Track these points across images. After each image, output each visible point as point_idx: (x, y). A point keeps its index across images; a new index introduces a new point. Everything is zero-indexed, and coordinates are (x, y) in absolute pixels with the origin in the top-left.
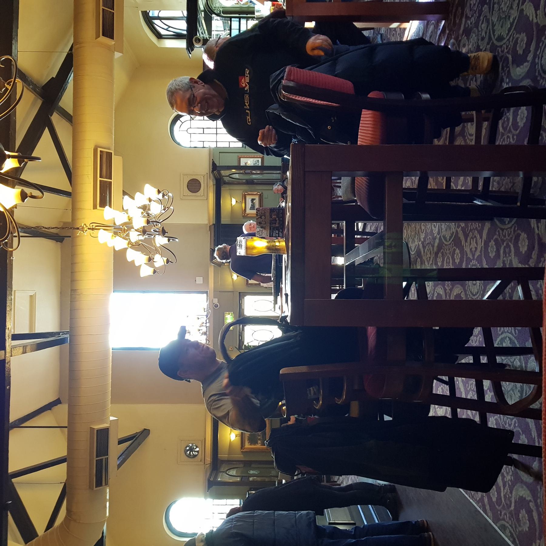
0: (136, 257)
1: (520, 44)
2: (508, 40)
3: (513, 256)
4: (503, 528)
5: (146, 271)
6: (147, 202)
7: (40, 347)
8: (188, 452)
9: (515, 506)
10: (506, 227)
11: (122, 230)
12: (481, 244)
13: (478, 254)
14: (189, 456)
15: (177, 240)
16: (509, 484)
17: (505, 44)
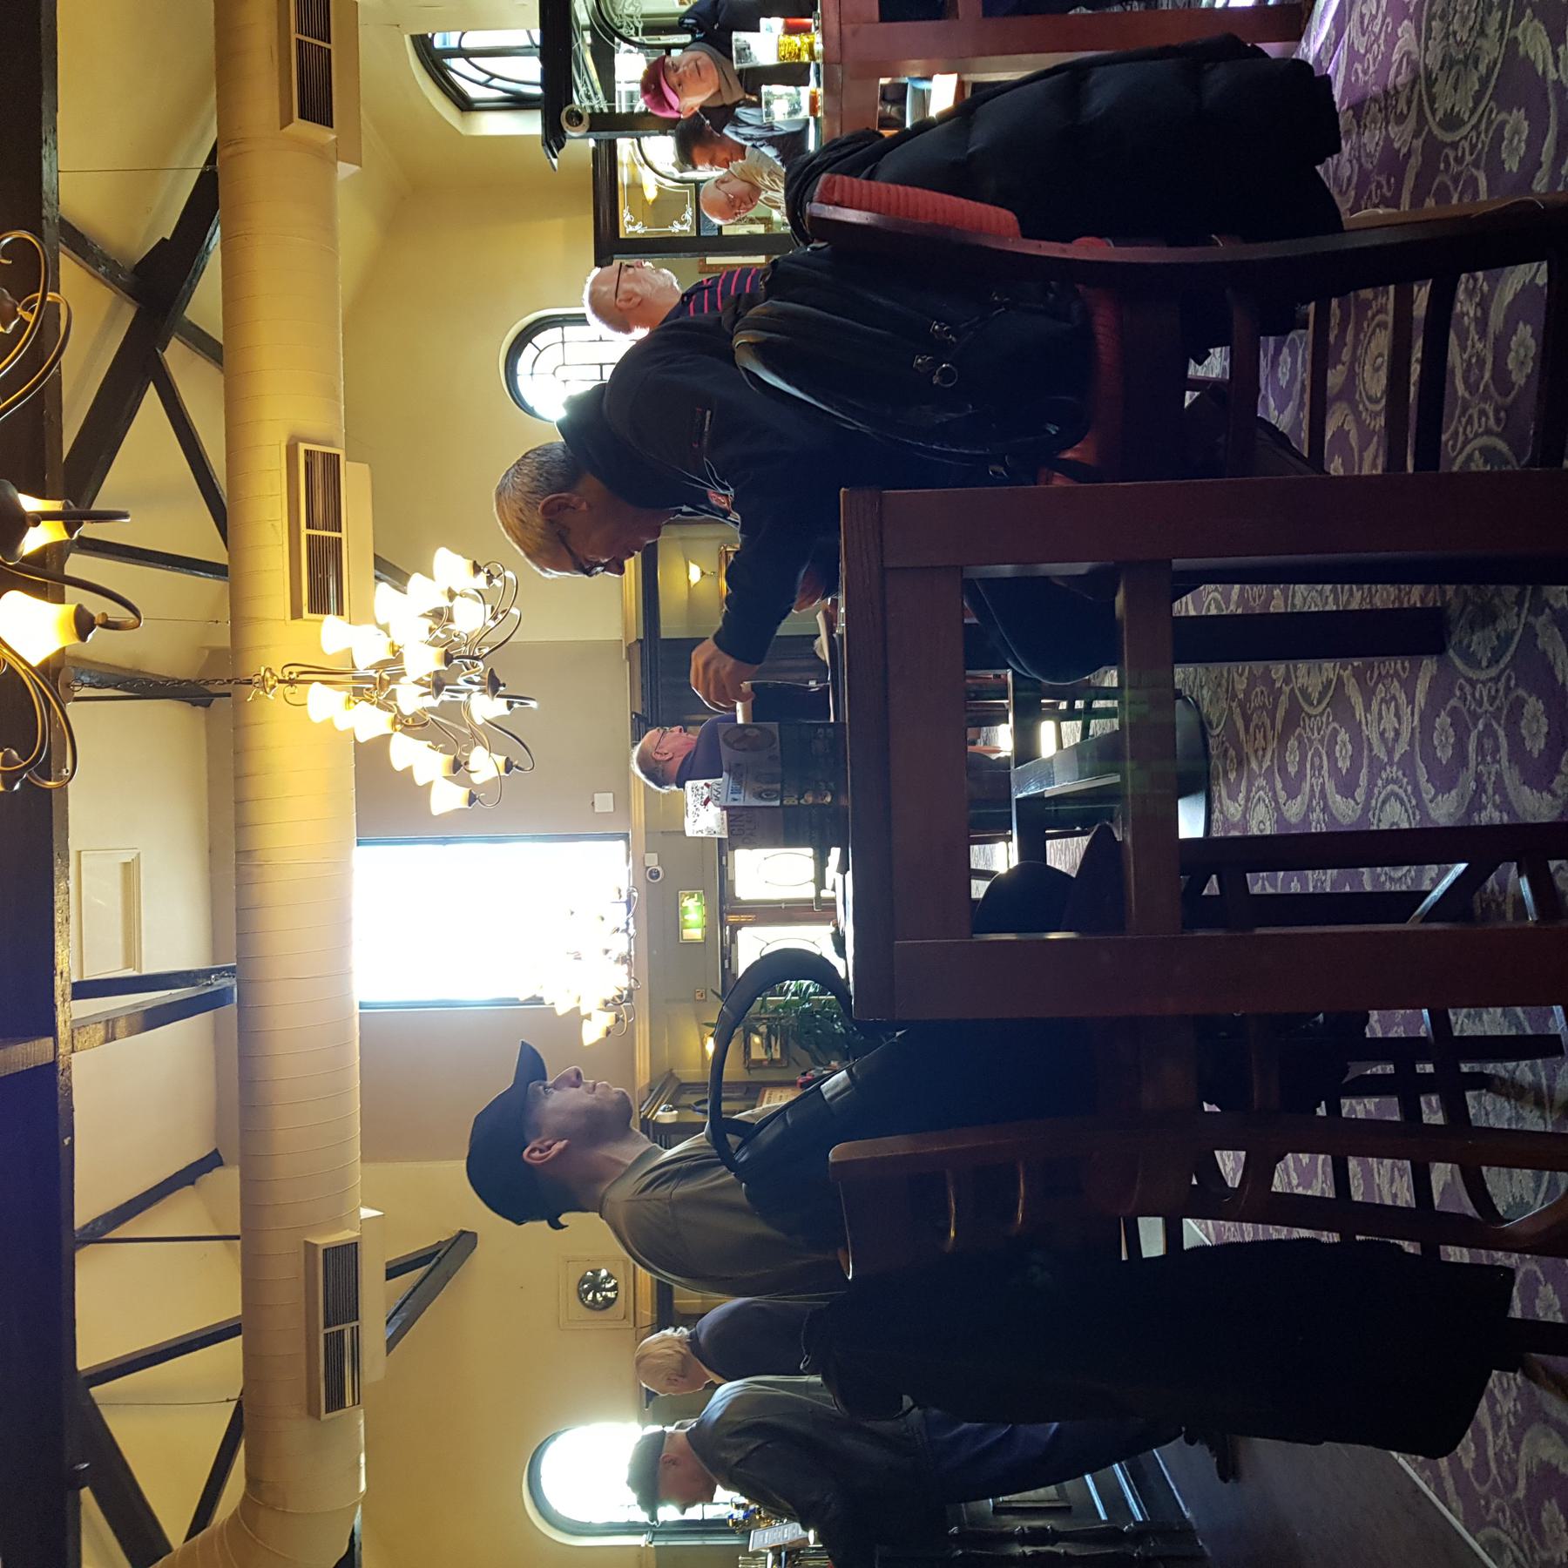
0: (417, 759)
1: (1511, 141)
2: (1476, 127)
3: (1505, 763)
5: (447, 798)
6: (443, 602)
7: (154, 1018)
8: (590, 1296)
11: (375, 685)
12: (1411, 721)
13: (1402, 748)
14: (594, 1306)
15: (533, 704)
17: (1465, 138)
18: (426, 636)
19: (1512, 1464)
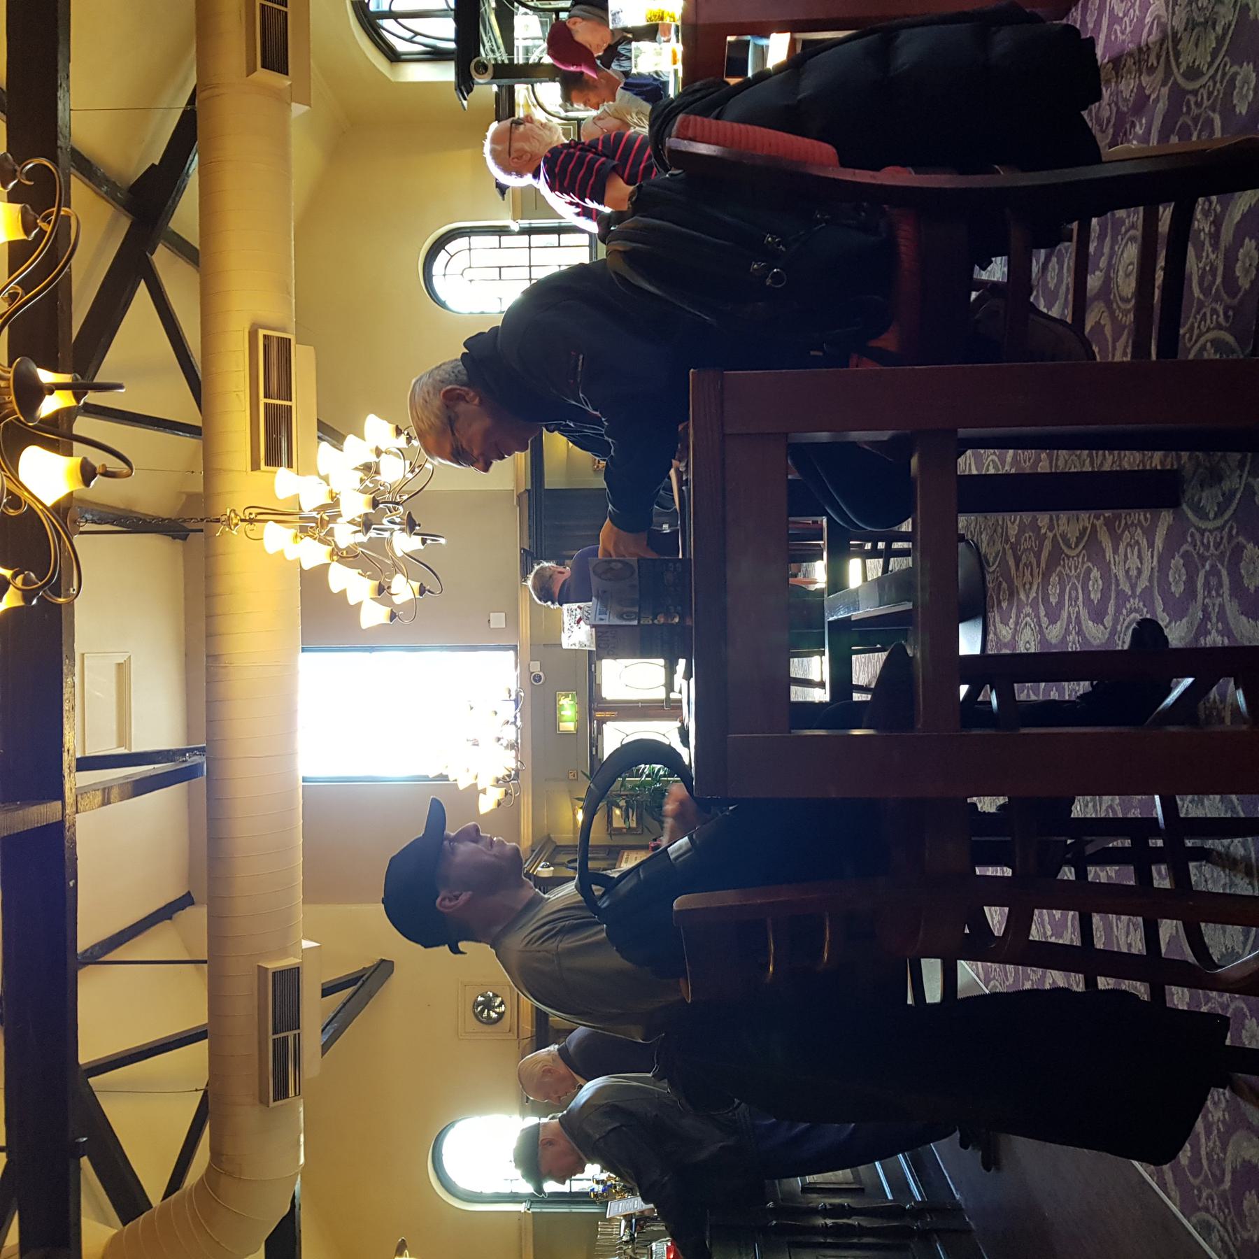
0: (349, 583)
1: (1242, 88)
2: (1213, 77)
4: (1205, 1228)
5: (373, 615)
6: (372, 458)
9: (1233, 1181)
10: (1210, 336)
11: (316, 525)
12: (1150, 563)
13: (1143, 583)
15: (442, 541)
16: (1218, 1129)
17: (1204, 86)
18: (358, 485)
19: (1220, 1162)
